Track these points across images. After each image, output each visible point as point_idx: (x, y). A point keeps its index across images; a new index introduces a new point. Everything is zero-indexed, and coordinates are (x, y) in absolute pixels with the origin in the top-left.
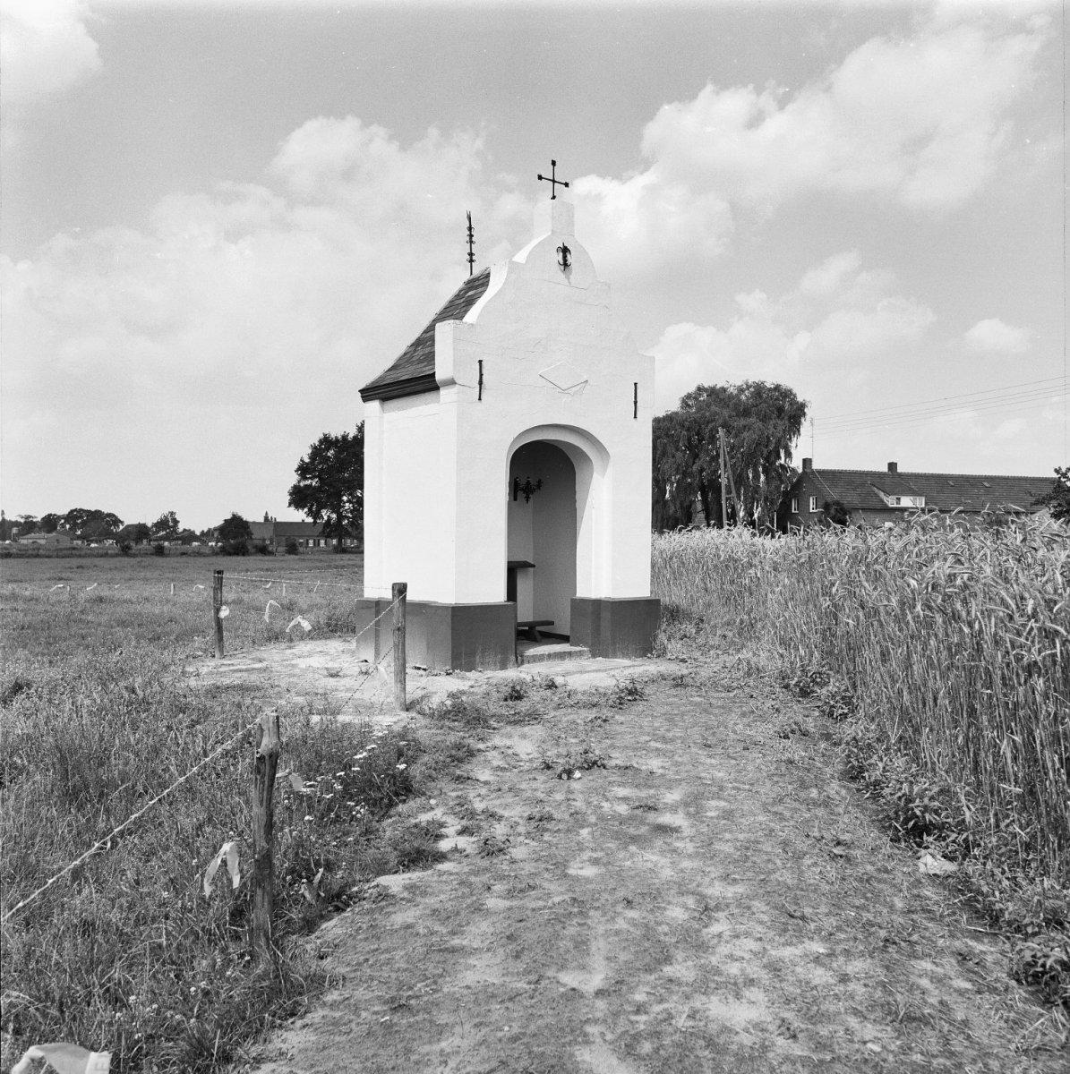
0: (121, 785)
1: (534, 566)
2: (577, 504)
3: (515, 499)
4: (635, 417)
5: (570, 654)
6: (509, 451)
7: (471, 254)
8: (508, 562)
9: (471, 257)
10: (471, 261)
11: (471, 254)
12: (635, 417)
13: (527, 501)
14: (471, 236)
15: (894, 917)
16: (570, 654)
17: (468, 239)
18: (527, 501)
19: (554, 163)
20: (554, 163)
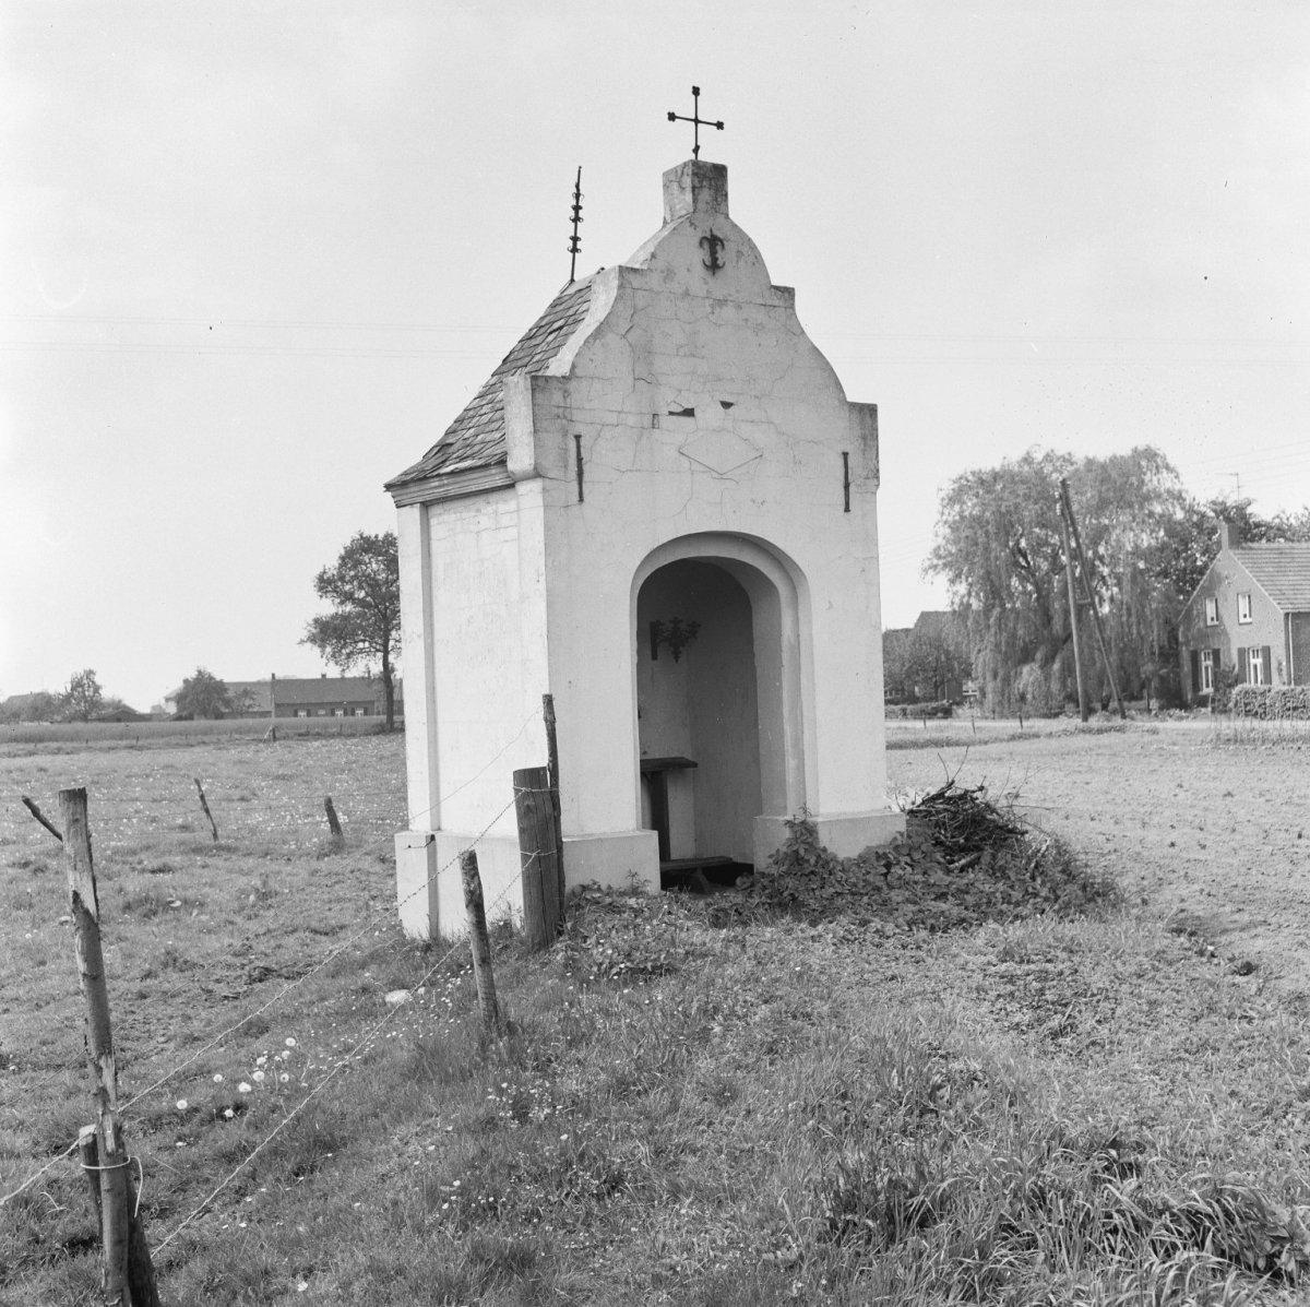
0: (1194, 589)
1: (695, 765)
2: (757, 657)
3: (654, 657)
4: (847, 509)
5: (54, 738)
6: (631, 596)
7: (575, 239)
8: (642, 762)
9: (575, 244)
10: (575, 250)
11: (575, 239)
12: (847, 509)
13: (677, 658)
14: (577, 208)
15: (1071, 1293)
16: (54, 738)
17: (572, 214)
18: (677, 658)
19: (696, 91)
20: (696, 91)
